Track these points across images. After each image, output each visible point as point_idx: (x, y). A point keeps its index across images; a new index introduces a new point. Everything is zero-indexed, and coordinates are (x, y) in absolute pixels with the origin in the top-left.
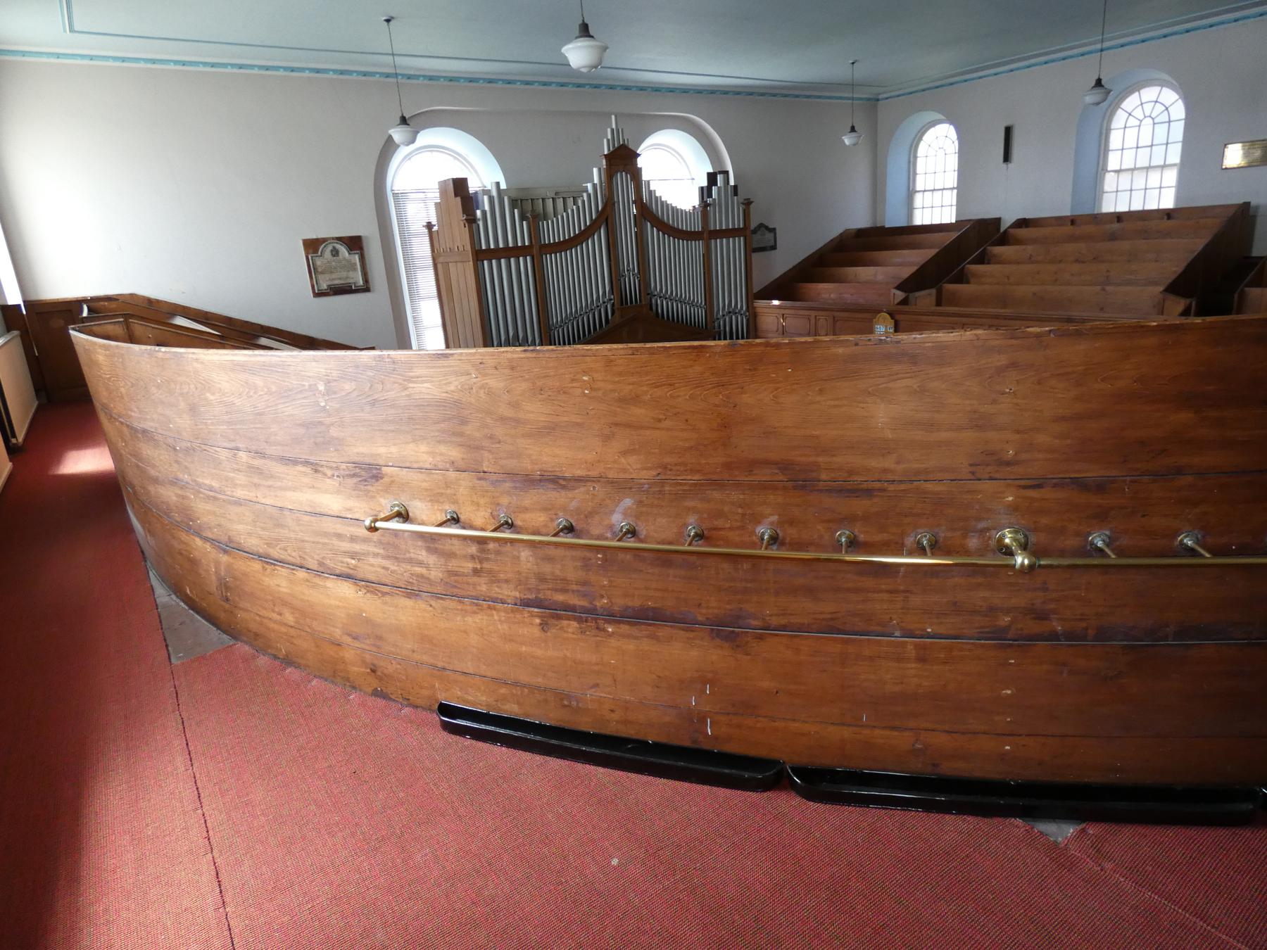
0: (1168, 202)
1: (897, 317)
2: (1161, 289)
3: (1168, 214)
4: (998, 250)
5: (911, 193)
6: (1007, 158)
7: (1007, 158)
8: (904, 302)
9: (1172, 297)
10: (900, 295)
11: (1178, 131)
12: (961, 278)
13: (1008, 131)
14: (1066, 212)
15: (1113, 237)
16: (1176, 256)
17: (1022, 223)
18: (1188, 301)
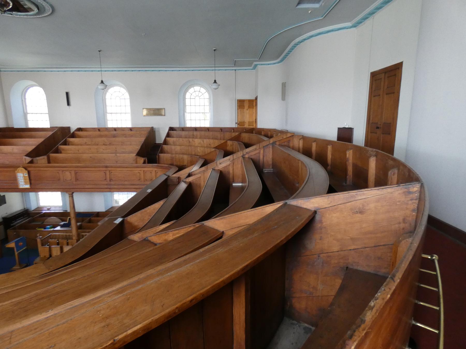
0: (130, 126)
1: (29, 169)
2: (135, 154)
3: (131, 129)
4: (72, 140)
5: (25, 115)
6: (68, 104)
7: (68, 104)
8: (31, 162)
9: (139, 157)
10: (29, 159)
11: (128, 102)
12: (57, 151)
13: (67, 94)
14: (96, 126)
15: (114, 136)
16: (137, 143)
17: (79, 129)
18: (144, 158)
